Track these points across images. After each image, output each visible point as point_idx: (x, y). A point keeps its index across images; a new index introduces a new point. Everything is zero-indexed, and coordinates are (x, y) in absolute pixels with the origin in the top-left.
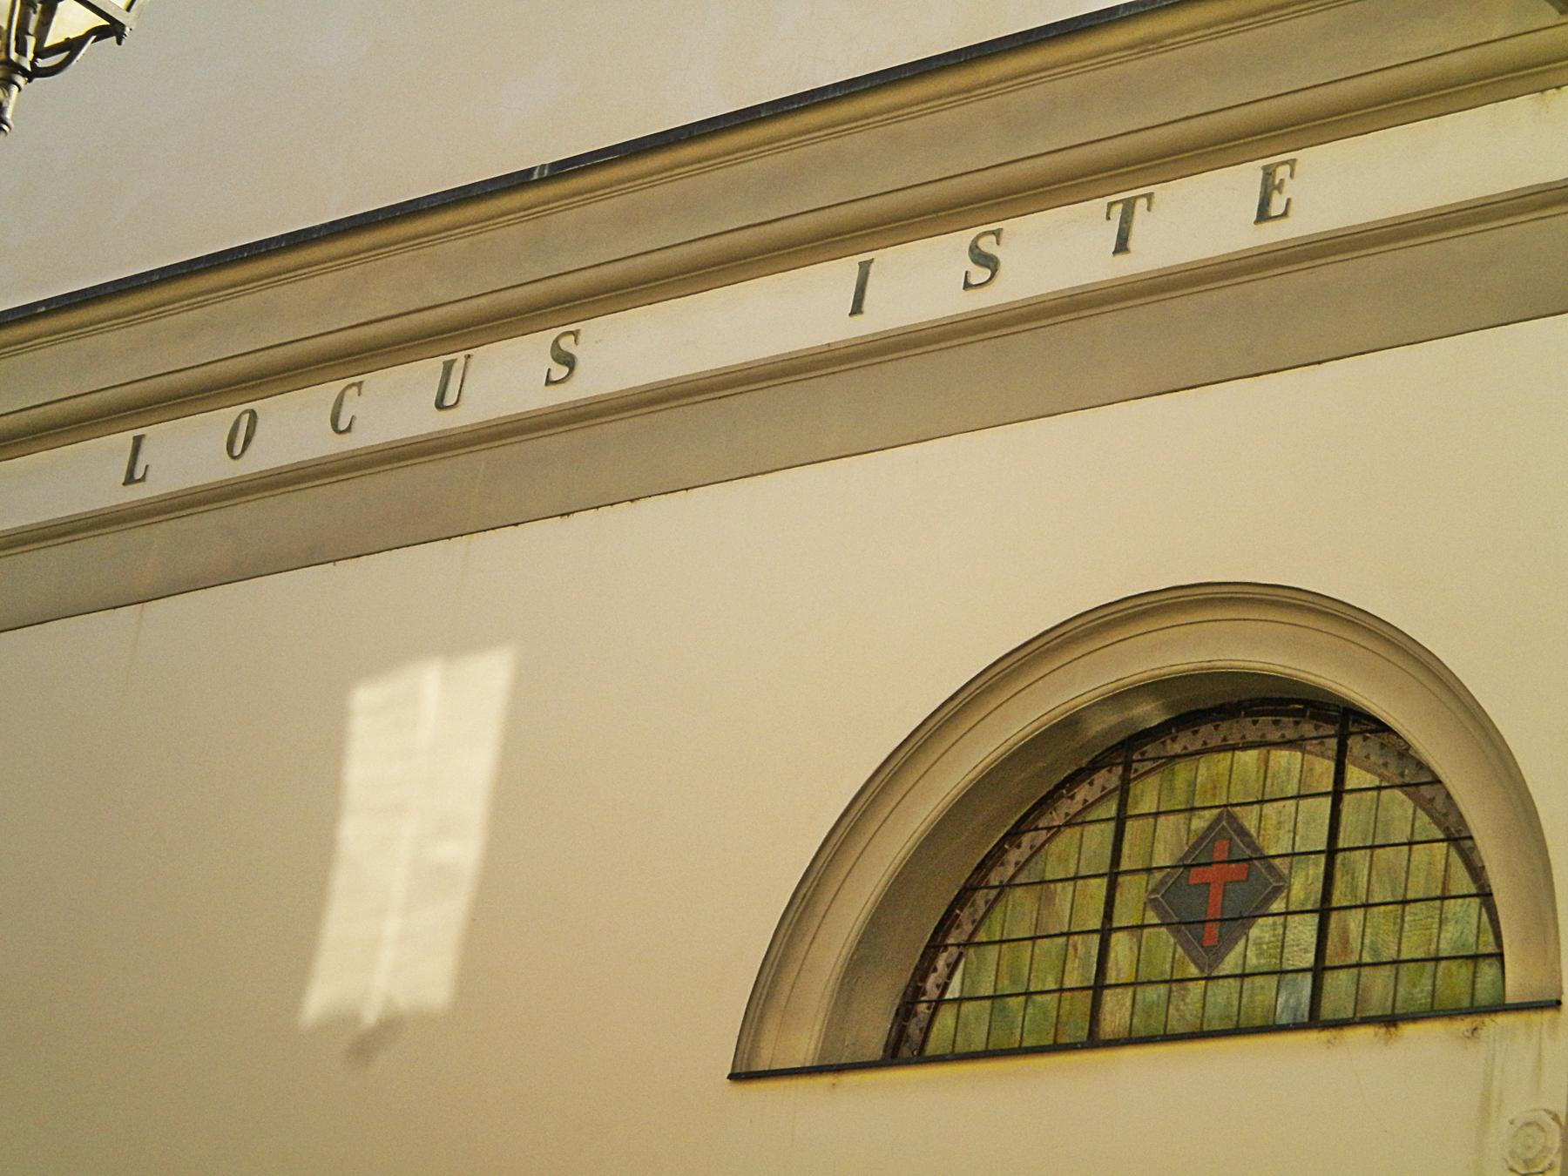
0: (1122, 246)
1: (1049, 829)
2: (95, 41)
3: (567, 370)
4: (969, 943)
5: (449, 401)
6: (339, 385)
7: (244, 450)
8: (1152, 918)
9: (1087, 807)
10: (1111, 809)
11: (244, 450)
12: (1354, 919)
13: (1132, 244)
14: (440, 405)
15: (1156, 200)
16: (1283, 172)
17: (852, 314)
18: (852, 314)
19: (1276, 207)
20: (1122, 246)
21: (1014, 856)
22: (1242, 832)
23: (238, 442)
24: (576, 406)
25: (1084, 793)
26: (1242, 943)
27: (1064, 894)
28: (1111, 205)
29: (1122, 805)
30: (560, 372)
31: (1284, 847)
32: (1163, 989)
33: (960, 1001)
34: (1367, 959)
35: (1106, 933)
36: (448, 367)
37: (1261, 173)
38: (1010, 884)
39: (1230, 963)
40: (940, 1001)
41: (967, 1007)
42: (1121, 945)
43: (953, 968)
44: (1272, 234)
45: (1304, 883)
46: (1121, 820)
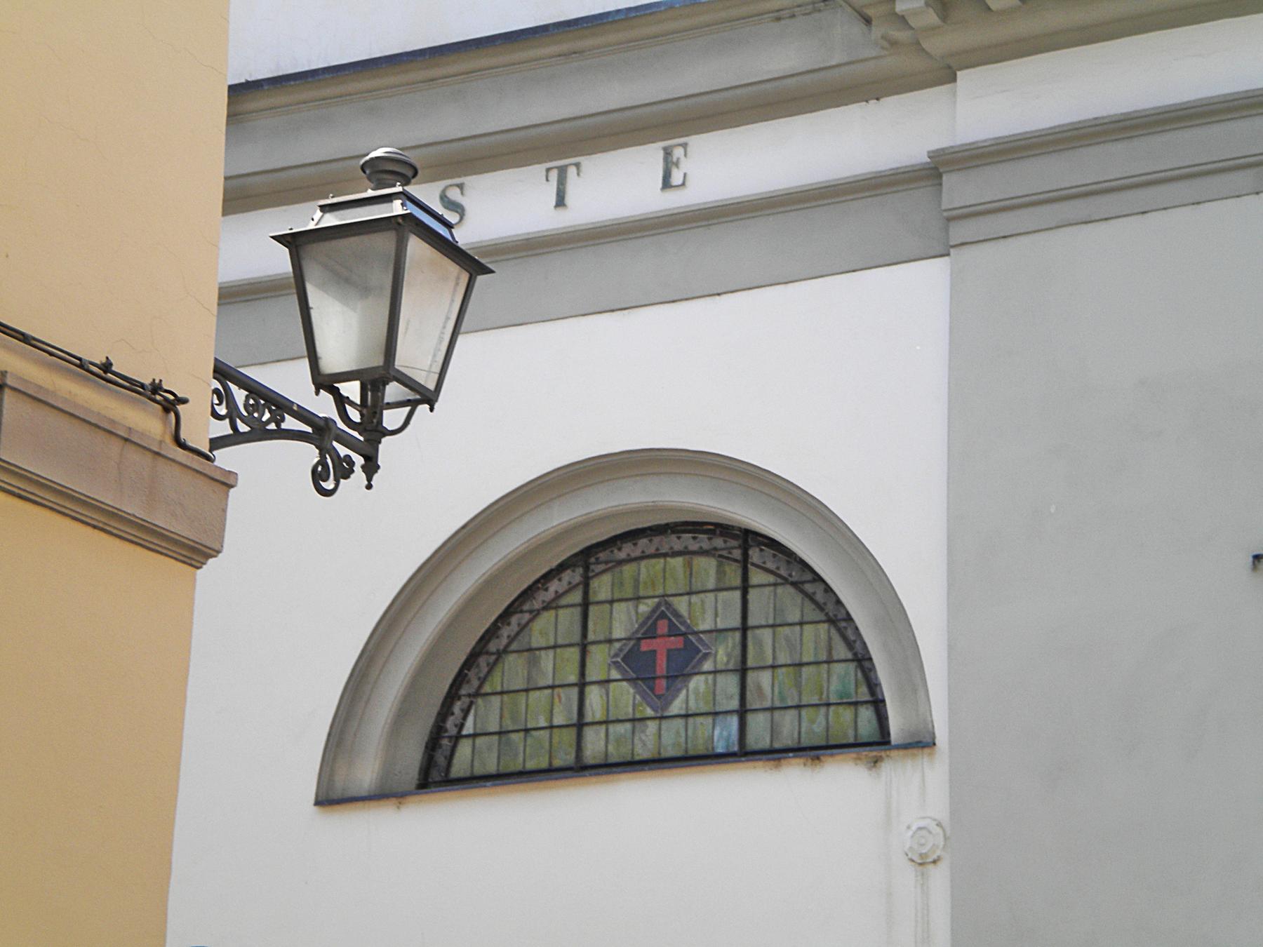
4: (477, 694)
8: (615, 674)
9: (558, 596)
10: (576, 597)
12: (765, 678)
16: (678, 152)
21: (506, 632)
22: (677, 615)
25: (554, 586)
26: (684, 692)
27: (547, 660)
28: (548, 170)
29: (586, 594)
31: (705, 625)
32: (628, 726)
33: (474, 736)
34: (777, 704)
35: (582, 685)
38: (506, 651)
39: (676, 707)
40: (458, 737)
41: (480, 741)
42: (594, 696)
43: (466, 712)
45: (724, 653)
46: (585, 605)
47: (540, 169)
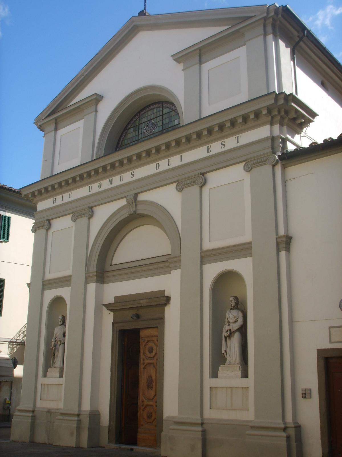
0: (238, 142)
1: (128, 129)
2: (266, 5)
3: (224, 146)
5: (122, 180)
6: (69, 193)
7: (158, 168)
11: (158, 168)
13: (239, 142)
14: (120, 181)
15: (241, 136)
16: (209, 147)
17: (237, 143)
18: (237, 143)
19: (209, 151)
20: (238, 142)
23: (157, 167)
24: (159, 172)
28: (235, 138)
30: (132, 176)
36: (121, 176)
37: (168, 161)
44: (170, 167)
47: (234, 137)
